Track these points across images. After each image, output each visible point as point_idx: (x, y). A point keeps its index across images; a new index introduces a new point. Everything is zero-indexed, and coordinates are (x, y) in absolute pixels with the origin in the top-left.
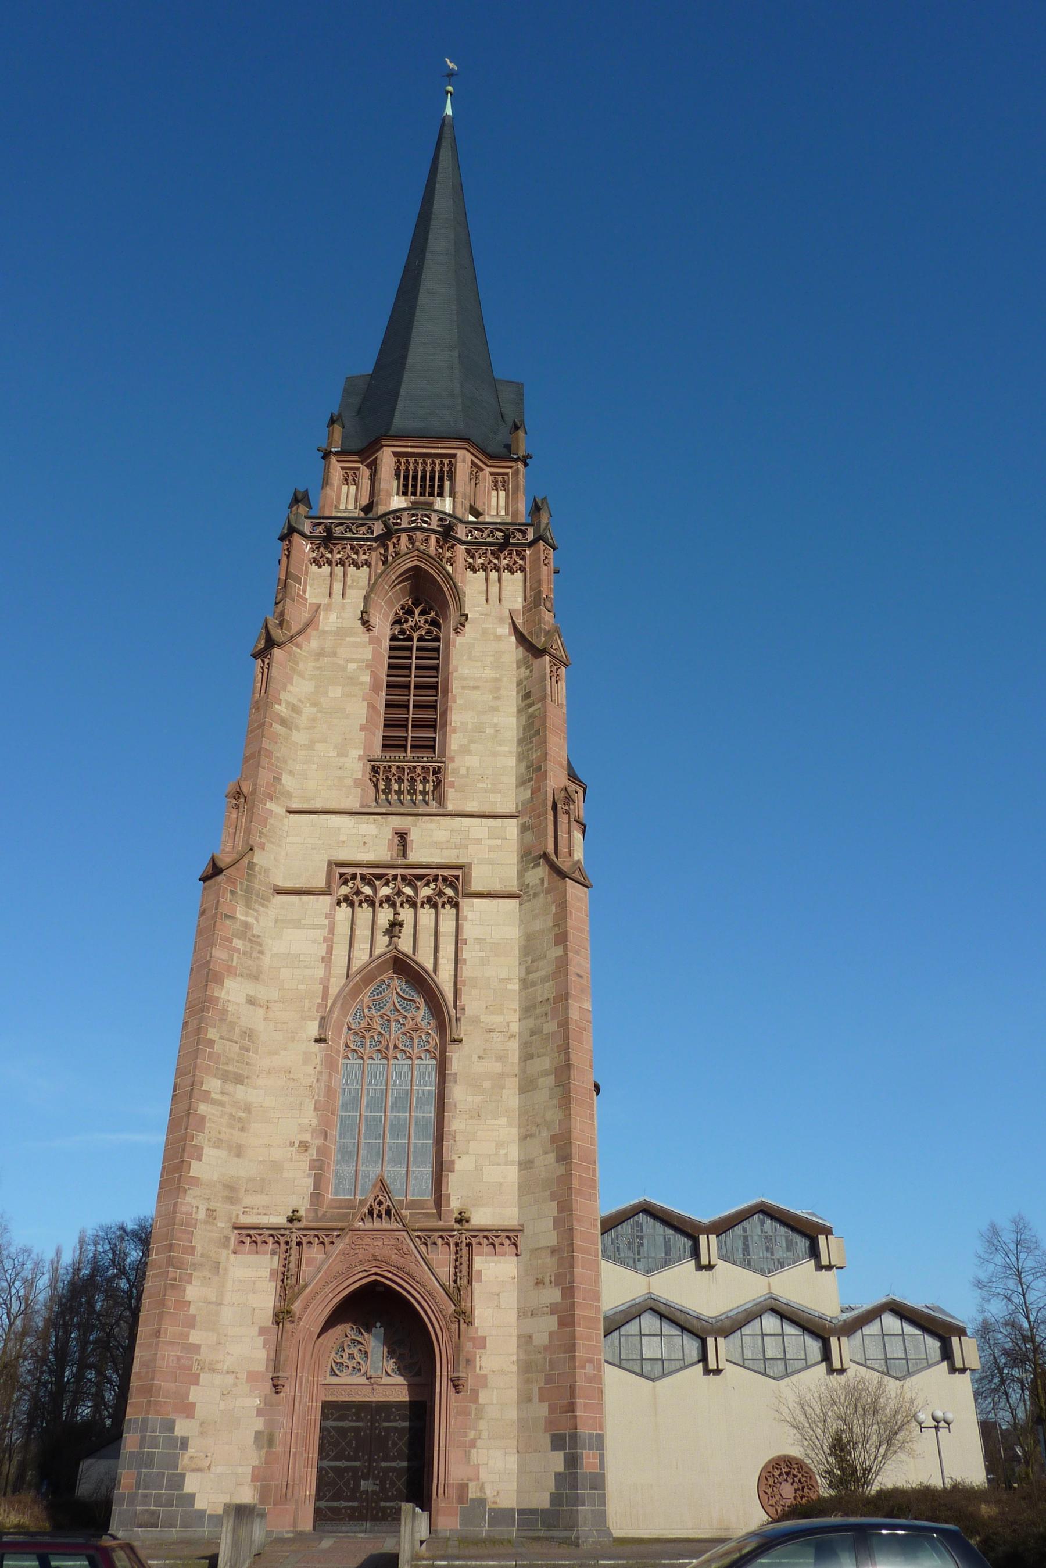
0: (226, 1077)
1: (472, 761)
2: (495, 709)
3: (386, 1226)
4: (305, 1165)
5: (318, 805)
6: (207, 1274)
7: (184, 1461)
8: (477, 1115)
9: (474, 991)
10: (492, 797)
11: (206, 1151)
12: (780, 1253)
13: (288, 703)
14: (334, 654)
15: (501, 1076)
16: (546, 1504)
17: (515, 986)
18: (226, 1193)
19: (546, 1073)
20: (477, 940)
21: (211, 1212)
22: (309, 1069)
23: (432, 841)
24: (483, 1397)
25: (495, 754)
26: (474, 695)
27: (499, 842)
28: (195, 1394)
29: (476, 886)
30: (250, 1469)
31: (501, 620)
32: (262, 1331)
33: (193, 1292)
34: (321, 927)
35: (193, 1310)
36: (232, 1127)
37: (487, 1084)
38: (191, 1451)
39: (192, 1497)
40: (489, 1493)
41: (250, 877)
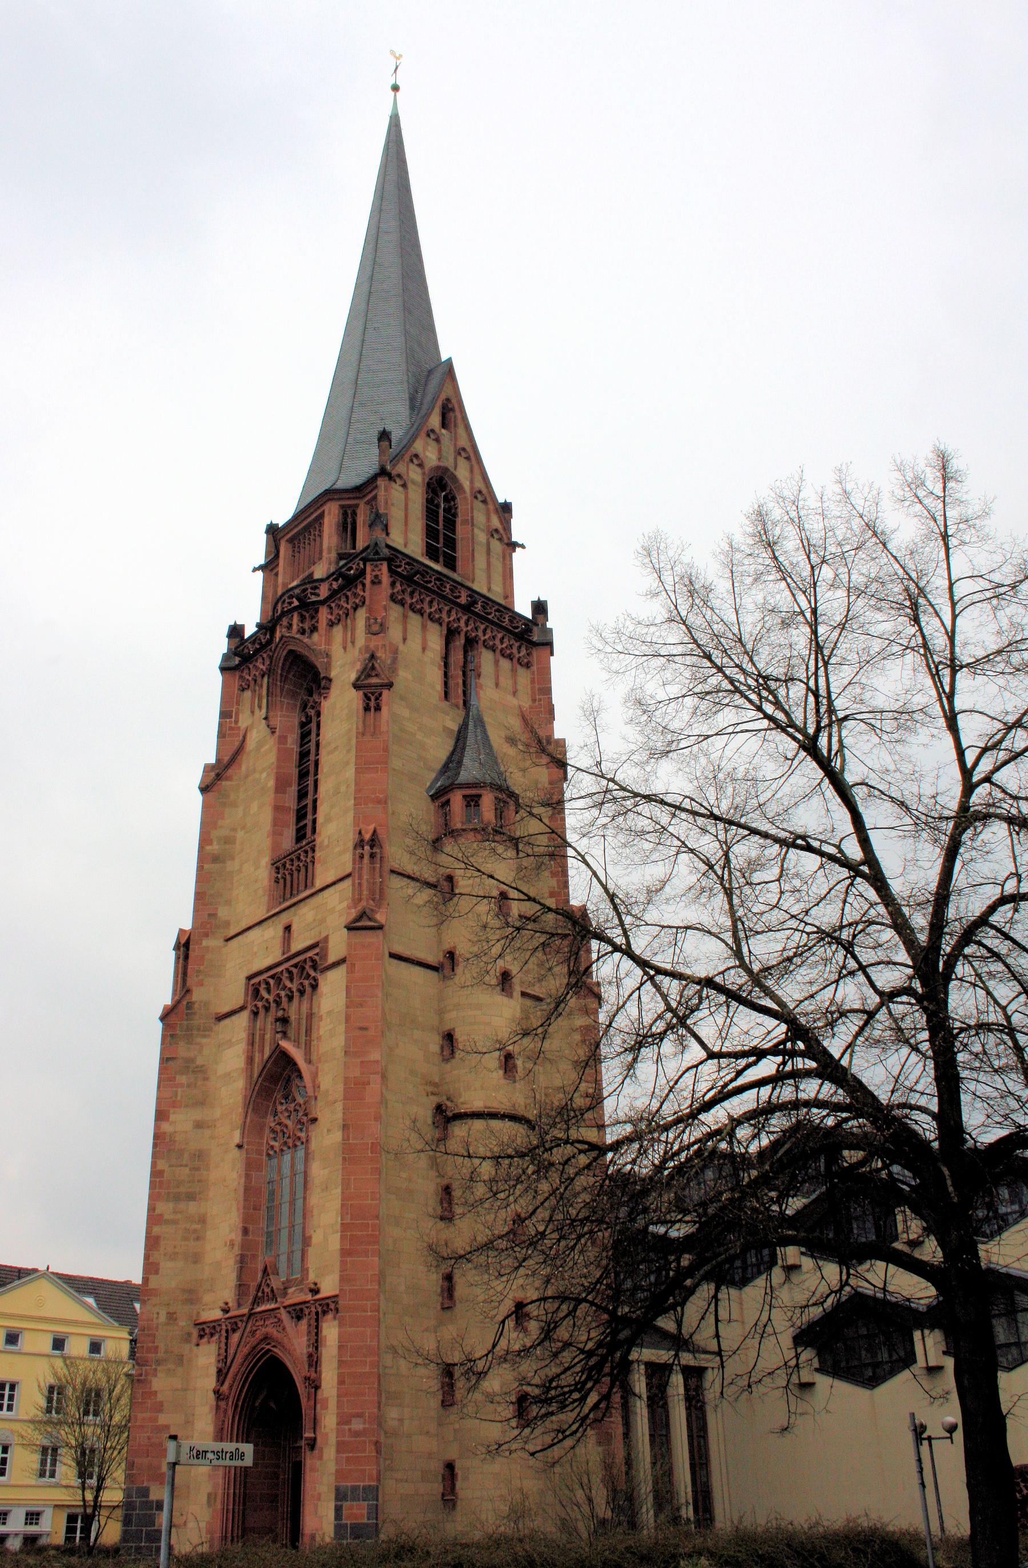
6: (171, 1366)
11: (162, 1264)
21: (172, 1317)
22: (234, 1175)
36: (186, 1239)
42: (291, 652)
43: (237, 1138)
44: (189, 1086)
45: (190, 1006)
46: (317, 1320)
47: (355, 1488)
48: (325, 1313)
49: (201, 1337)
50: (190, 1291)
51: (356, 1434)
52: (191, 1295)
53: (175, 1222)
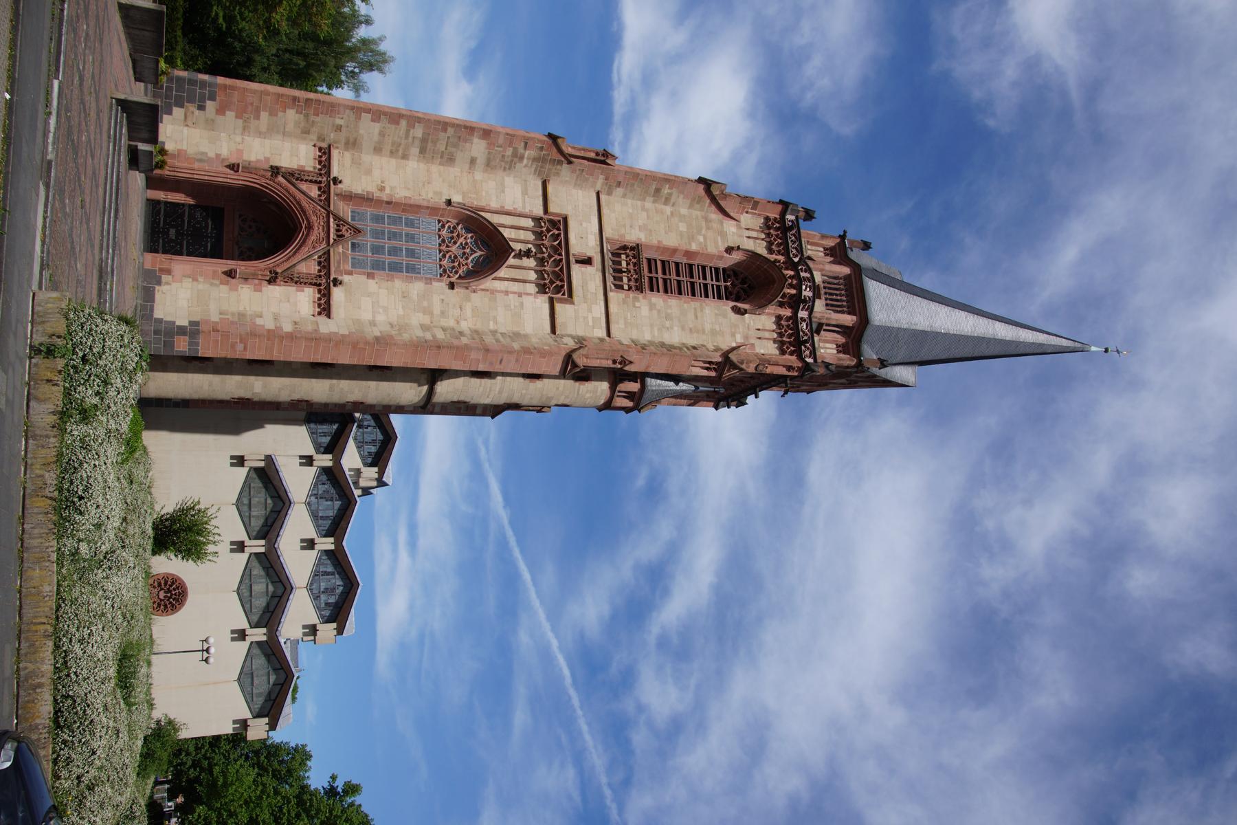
0: (424, 140)
1: (645, 310)
2: (683, 328)
3: (332, 236)
4: (369, 189)
5: (605, 211)
6: (303, 124)
7: (192, 108)
8: (405, 296)
9: (486, 300)
10: (622, 322)
11: (378, 125)
12: (323, 597)
13: (670, 194)
14: (708, 228)
15: (431, 314)
16: (156, 316)
17: (492, 326)
18: (351, 140)
19: (434, 336)
20: (522, 304)
21: (339, 128)
22: (430, 195)
23: (586, 280)
24: (224, 288)
25: (652, 326)
26: (691, 316)
27: (591, 323)
28: (230, 115)
29: (559, 307)
30: (184, 147)
31: (746, 337)
32: (267, 159)
33: (291, 115)
34: (524, 207)
35: (280, 114)
36: (393, 144)
37: (425, 304)
38: (197, 112)
39: (170, 113)
40: (164, 288)
41: (553, 162)
42: (774, 282)
43: (456, 199)
44: (503, 156)
45: (560, 162)
46: (316, 182)
47: (197, 344)
48: (319, 291)
49: (320, 149)
50: (354, 143)
51: (233, 346)
52: (352, 144)
53: (407, 137)
